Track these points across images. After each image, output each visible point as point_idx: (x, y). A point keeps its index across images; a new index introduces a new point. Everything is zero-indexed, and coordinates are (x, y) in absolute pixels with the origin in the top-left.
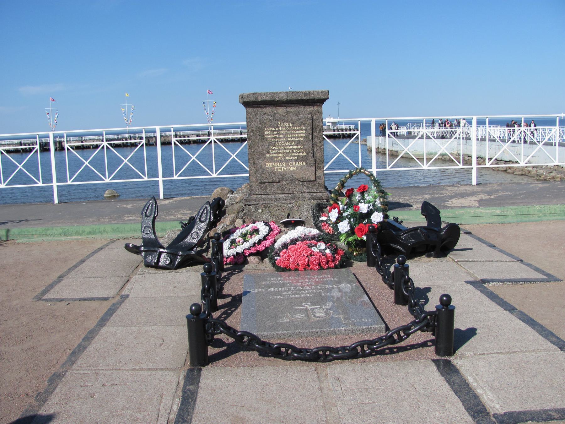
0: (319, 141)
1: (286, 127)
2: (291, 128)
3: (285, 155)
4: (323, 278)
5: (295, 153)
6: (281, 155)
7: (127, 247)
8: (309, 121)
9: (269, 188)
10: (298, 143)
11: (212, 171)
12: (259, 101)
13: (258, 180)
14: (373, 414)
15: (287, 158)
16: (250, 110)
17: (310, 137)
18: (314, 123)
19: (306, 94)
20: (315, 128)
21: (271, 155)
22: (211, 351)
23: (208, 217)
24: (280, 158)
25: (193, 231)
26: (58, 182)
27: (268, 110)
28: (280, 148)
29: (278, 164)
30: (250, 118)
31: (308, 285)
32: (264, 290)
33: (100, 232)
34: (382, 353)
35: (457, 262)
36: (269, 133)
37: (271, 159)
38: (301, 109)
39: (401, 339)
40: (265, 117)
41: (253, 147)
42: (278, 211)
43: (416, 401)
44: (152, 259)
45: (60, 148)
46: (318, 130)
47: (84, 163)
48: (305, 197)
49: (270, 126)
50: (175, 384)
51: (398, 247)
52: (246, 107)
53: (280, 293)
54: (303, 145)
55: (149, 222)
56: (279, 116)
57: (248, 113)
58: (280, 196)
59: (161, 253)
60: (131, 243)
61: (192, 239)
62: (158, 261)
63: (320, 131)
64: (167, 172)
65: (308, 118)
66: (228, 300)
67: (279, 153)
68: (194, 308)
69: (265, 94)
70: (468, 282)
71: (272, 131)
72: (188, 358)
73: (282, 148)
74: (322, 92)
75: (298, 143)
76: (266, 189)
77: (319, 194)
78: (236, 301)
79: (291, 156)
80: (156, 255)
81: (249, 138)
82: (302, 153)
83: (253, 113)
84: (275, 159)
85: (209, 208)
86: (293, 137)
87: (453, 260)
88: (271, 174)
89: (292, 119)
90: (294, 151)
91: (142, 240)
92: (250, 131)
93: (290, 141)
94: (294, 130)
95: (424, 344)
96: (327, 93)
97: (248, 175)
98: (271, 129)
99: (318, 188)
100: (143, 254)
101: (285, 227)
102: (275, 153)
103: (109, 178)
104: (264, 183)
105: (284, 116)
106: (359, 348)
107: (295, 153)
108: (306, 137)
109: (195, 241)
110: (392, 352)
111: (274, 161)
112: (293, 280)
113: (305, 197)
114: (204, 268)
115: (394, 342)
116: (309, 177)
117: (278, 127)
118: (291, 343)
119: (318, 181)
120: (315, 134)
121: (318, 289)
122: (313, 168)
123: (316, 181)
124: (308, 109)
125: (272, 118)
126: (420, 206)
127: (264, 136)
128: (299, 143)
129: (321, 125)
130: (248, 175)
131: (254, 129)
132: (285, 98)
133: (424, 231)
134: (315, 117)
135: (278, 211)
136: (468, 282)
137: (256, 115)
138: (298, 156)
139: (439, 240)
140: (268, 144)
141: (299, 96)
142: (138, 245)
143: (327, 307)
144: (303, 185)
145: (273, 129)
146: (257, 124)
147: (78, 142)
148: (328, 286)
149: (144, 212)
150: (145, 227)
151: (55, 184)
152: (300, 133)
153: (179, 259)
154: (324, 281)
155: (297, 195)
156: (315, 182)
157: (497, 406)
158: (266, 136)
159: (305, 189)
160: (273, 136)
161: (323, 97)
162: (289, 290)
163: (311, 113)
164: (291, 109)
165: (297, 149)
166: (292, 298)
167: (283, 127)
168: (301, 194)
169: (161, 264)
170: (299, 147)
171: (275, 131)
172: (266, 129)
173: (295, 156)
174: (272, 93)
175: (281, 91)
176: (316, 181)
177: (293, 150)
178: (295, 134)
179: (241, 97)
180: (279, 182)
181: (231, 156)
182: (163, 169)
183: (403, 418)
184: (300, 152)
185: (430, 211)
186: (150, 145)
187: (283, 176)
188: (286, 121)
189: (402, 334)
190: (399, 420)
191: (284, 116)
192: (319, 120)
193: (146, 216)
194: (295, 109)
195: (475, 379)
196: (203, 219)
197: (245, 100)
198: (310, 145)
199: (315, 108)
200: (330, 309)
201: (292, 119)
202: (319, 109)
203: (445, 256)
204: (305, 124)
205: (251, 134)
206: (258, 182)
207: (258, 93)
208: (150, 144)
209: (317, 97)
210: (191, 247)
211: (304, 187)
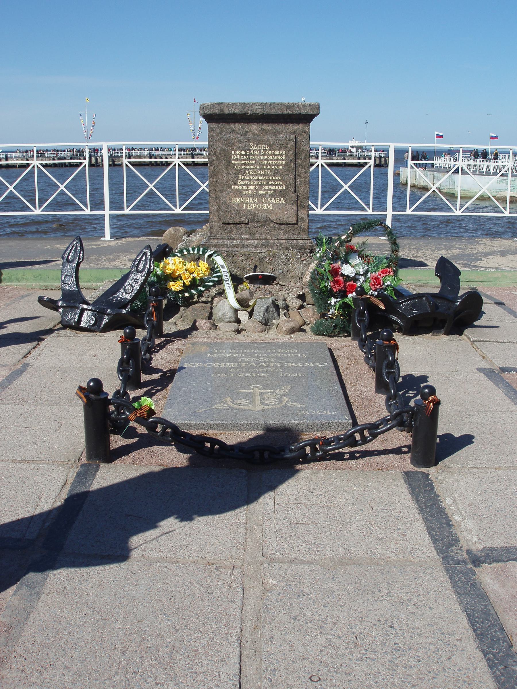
0: (303, 171)
1: (260, 150)
2: (267, 152)
3: (257, 187)
4: (287, 353)
5: (271, 185)
6: (252, 188)
7: (41, 300)
8: (292, 144)
9: (234, 231)
10: (276, 172)
11: (175, 207)
12: (224, 114)
13: (220, 219)
14: (307, 538)
15: (260, 192)
16: (214, 125)
17: (292, 165)
18: (297, 147)
19: (288, 107)
20: (299, 154)
21: (239, 187)
22: (117, 441)
23: (148, 266)
24: (250, 192)
25: (127, 284)
26: (111, 209)
27: (237, 126)
28: (251, 178)
29: (247, 200)
30: (213, 136)
31: (265, 362)
32: (197, 365)
33: (17, 279)
34: (340, 457)
35: (473, 341)
36: (236, 156)
37: (239, 193)
38: (281, 127)
39: (365, 441)
40: (233, 136)
41: (216, 175)
42: (244, 262)
43: (369, 525)
44: (72, 317)
45: (115, 164)
46: (303, 155)
47: (346, 184)
48: (281, 245)
49: (238, 148)
50: (61, 483)
51: (395, 318)
52: (208, 122)
53: (225, 370)
54: (282, 175)
55: (70, 269)
56: (251, 135)
57: (210, 130)
58: (249, 241)
59: (83, 310)
60: (48, 295)
61: (126, 294)
62: (79, 320)
63: (305, 158)
64: (116, 205)
65: (290, 140)
66: (157, 376)
67: (250, 185)
68: (92, 384)
69: (234, 105)
70: (480, 370)
71: (241, 154)
72: (85, 451)
73: (254, 178)
74: (310, 105)
75: (276, 172)
76: (231, 231)
77: (300, 241)
78: (168, 377)
79: (265, 190)
80: (78, 311)
81: (211, 164)
82: (281, 185)
83: (218, 130)
84: (244, 193)
85: (149, 254)
86: (270, 164)
87: (469, 339)
88: (238, 212)
89: (268, 140)
90: (270, 183)
91: (60, 293)
92: (212, 154)
93: (265, 169)
94: (271, 155)
95: (397, 451)
96: (317, 107)
97: (208, 212)
98: (240, 152)
99: (299, 234)
100: (61, 310)
101: (250, 283)
102: (244, 185)
103: (40, 207)
104: (229, 224)
105: (258, 135)
106: (257, 454)
107: (271, 185)
108: (286, 165)
109: (128, 297)
110: (353, 456)
111: (243, 196)
112: (248, 353)
113: (281, 245)
114: (125, 332)
115: (355, 444)
116: (288, 218)
117: (250, 151)
118: (219, 438)
119: (300, 224)
120: (299, 161)
121: (277, 367)
122: (294, 207)
123: (297, 224)
124: (291, 127)
125: (242, 138)
126: (433, 264)
127: (230, 162)
128: (277, 173)
129: (308, 149)
130: (208, 212)
131: (218, 151)
132: (260, 111)
133: (431, 299)
134: (299, 139)
135: (244, 262)
136: (480, 370)
137: (221, 132)
138: (275, 190)
139: (453, 312)
140: (235, 171)
141: (279, 109)
142: (56, 299)
143: (282, 392)
144: (279, 229)
145: (244, 153)
146: (221, 145)
147: (22, 160)
148: (290, 364)
149: (66, 256)
150: (66, 275)
151: (107, 212)
152: (279, 159)
153: (106, 320)
154: (287, 357)
155: (271, 241)
156: (296, 226)
157: (475, 539)
158: (233, 162)
159: (282, 235)
160: (242, 162)
161: (311, 112)
162: (240, 366)
163: (294, 133)
164: (268, 127)
165: (274, 181)
166: (240, 377)
167: (257, 149)
168: (276, 241)
169: (83, 324)
170: (277, 178)
171: (246, 155)
172: (233, 152)
173: (270, 190)
174: (244, 104)
175: (254, 102)
176: (297, 224)
177: (268, 181)
178: (272, 160)
179: (203, 107)
180: (248, 223)
181: (346, 184)
182: (110, 198)
183: (346, 546)
184: (277, 185)
185: (446, 270)
186: (115, 165)
187: (254, 215)
188: (261, 142)
189: (366, 433)
190: (341, 548)
191: (258, 135)
192: (305, 143)
193: (68, 261)
194: (274, 127)
195: (454, 501)
196: (140, 268)
197: (208, 112)
198: (291, 175)
199: (301, 126)
200: (285, 395)
201: (268, 140)
202: (306, 128)
203: (460, 333)
204: (286, 148)
205: (214, 158)
206: (221, 222)
207: (225, 104)
208: (96, 165)
209: (303, 112)
210: (123, 304)
211: (282, 232)
